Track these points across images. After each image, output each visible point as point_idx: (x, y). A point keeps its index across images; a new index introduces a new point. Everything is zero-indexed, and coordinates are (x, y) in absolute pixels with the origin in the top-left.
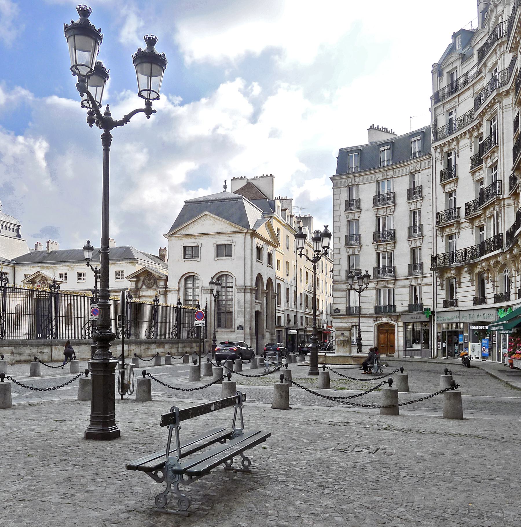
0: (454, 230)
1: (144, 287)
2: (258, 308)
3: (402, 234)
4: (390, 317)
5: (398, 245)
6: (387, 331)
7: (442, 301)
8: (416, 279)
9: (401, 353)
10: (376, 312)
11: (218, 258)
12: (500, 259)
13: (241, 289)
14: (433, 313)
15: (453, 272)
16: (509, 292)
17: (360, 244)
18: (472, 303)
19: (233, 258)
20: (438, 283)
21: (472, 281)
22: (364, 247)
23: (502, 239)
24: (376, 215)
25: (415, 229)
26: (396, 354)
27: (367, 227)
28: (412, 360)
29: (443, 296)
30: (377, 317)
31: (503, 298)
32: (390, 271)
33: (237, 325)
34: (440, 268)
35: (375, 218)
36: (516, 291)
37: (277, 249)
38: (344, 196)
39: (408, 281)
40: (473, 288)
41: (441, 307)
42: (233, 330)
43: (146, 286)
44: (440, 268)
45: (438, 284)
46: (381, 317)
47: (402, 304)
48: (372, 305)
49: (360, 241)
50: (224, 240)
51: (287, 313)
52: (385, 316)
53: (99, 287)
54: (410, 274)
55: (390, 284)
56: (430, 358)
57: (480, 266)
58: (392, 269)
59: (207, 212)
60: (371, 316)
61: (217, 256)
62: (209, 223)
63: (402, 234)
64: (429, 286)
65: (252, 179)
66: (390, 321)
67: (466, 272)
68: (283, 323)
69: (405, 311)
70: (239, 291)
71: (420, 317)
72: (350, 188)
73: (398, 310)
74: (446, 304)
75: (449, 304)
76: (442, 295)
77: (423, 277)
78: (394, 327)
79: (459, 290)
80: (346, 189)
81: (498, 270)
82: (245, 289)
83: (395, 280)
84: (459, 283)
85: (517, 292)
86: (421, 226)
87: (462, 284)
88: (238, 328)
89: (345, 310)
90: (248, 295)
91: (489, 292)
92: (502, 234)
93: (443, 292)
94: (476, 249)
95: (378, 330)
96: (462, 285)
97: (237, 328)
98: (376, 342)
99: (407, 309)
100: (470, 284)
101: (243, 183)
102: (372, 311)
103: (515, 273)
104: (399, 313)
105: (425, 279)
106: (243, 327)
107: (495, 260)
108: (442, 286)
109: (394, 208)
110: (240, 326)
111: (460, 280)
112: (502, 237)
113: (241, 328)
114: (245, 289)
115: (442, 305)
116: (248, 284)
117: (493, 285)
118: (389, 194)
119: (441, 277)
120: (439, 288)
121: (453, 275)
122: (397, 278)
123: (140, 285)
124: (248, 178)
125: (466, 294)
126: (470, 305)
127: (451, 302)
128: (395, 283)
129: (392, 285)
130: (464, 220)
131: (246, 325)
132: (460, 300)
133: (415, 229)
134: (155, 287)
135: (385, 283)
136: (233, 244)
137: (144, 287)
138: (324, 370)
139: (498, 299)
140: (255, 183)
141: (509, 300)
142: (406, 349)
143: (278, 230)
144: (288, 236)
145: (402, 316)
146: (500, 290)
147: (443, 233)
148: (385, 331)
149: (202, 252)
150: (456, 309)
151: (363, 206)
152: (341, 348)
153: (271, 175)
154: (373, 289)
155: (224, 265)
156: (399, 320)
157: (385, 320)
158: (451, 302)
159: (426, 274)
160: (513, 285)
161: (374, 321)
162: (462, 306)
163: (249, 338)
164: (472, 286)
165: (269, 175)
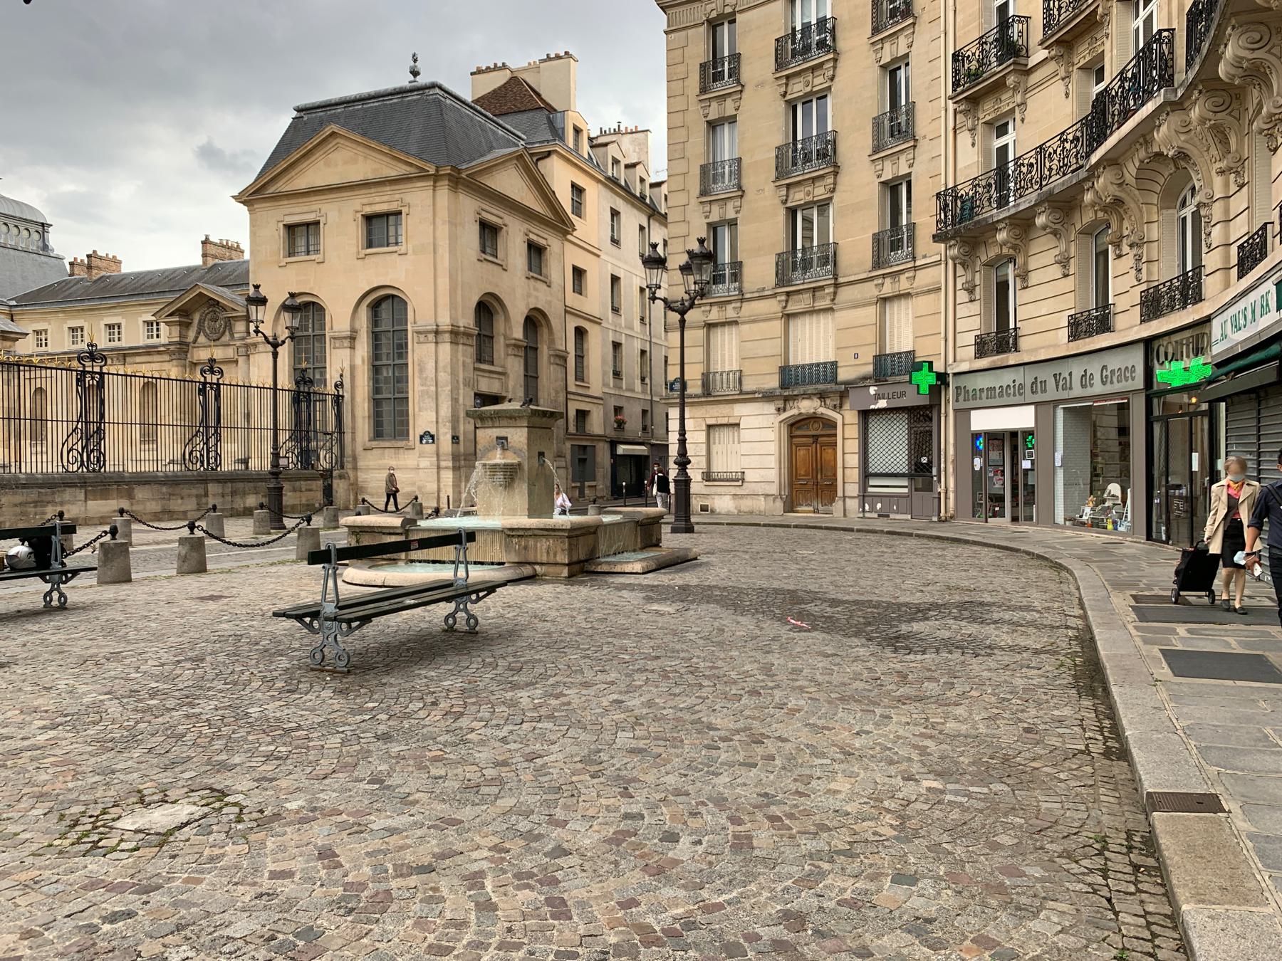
0: (1007, 101)
1: (202, 339)
2: (488, 385)
3: (855, 146)
4: (822, 396)
5: (843, 179)
6: (816, 437)
7: (970, 339)
8: (895, 275)
9: (853, 505)
10: (784, 386)
11: (369, 251)
12: (1163, 135)
13: (426, 333)
14: (942, 377)
15: (1002, 236)
16: (1198, 267)
17: (740, 188)
18: (1064, 333)
19: (402, 249)
20: (960, 282)
21: (1064, 262)
22: (750, 195)
23: (1171, 52)
24: (784, 95)
25: (896, 127)
26: (838, 506)
27: (760, 129)
28: (881, 524)
29: (975, 323)
30: (786, 399)
31: (1172, 299)
32: (824, 261)
33: (420, 431)
34: (963, 224)
35: (781, 106)
36: (1227, 257)
37: (569, 237)
38: (698, 50)
39: (871, 285)
40: (1069, 283)
41: (966, 359)
42: (411, 443)
43: (207, 335)
44: (963, 224)
45: (959, 286)
46: (794, 398)
47: (856, 356)
48: (774, 366)
49: (739, 179)
50: (381, 202)
51: (613, 402)
52: (808, 396)
53: (674, 413)
54: (878, 263)
55: (823, 297)
56: (935, 519)
57: (1088, 197)
58: (830, 258)
59: (334, 127)
60: (767, 397)
61: (370, 245)
62: (345, 162)
63: (855, 146)
64: (933, 296)
65: (524, 69)
66: (822, 410)
67: (1044, 228)
68: (597, 424)
69: (865, 378)
70: (422, 338)
71: (903, 394)
72: (714, 25)
73: (843, 375)
74: (982, 348)
75: (991, 346)
76: (973, 321)
77: (915, 268)
78: (834, 425)
79: (1024, 296)
80: (703, 29)
81: (1155, 199)
82: (437, 332)
83: (837, 285)
84: (1024, 276)
85: (1234, 260)
86: (735, 58)
87: (1032, 275)
88: (422, 437)
89: (700, 383)
90: (445, 348)
91: (1125, 290)
92: (1171, 30)
93: (976, 308)
94: (1076, 139)
95: (791, 437)
96: (1034, 278)
97: (418, 439)
98: (785, 471)
99: (869, 369)
100: (1056, 271)
101: (499, 79)
102: (773, 382)
103: (1227, 185)
104: (845, 383)
105: (920, 274)
106: (432, 437)
107: (1142, 154)
108: (971, 290)
109: (835, 68)
110: (427, 433)
111: (1026, 263)
112: (1171, 42)
113: (428, 437)
114: (437, 332)
115: (972, 350)
116: (445, 321)
117: (1138, 258)
118: (822, 22)
119: (965, 262)
120: (963, 296)
121: (1005, 250)
122: (841, 280)
123: (191, 334)
124: (513, 67)
125: (1044, 308)
126: (1060, 343)
127: (1001, 339)
128: (835, 293)
129: (828, 302)
130: (1041, 54)
131: (442, 430)
132: (1024, 328)
133: (896, 127)
134: (226, 338)
135: (807, 297)
136: (404, 210)
137: (202, 339)
138: (192, 533)
139: (1152, 305)
140: (530, 78)
141: (1199, 299)
142: (865, 490)
143: (577, 190)
144: (615, 213)
145: (852, 393)
146: (1166, 270)
147: (977, 118)
148: (811, 440)
149: (328, 237)
150: (1012, 358)
151: (747, 73)
152: (499, 499)
153: (566, 53)
154: (776, 319)
155: (388, 270)
156: (847, 406)
157: (807, 406)
158: (1001, 339)
159: (925, 257)
160: (1216, 232)
161: (779, 410)
162: (1032, 347)
163: (450, 464)
164: (1066, 276)
165: (562, 54)
